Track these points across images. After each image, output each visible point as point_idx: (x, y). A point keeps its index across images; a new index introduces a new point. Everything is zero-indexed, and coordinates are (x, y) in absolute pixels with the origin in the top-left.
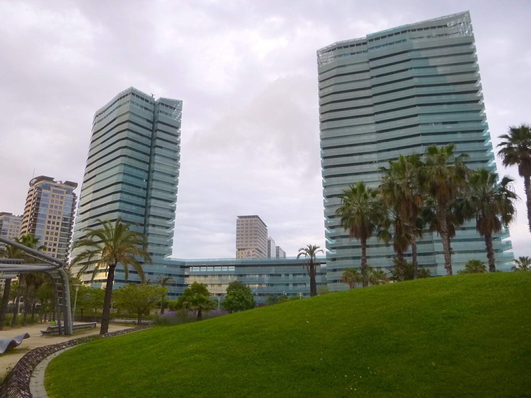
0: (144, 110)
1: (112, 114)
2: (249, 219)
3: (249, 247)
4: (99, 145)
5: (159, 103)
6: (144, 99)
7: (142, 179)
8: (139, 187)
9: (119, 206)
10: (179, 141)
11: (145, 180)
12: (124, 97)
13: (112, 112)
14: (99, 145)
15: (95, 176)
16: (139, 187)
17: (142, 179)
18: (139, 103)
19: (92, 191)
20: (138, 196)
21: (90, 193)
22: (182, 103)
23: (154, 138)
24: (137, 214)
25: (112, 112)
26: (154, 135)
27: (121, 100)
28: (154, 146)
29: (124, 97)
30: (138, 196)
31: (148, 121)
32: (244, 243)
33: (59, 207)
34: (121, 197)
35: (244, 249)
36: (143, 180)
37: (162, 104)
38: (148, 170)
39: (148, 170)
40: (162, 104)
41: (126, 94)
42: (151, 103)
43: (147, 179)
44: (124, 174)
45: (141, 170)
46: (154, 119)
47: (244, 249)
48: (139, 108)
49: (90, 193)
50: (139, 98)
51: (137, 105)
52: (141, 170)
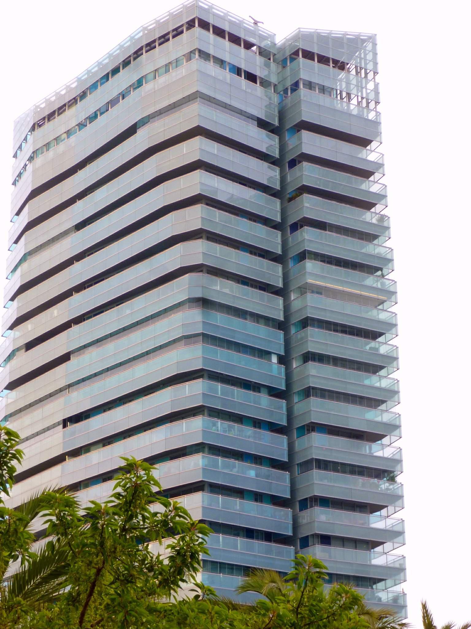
0: (243, 82)
1: (101, 120)
4: (65, 234)
5: (296, 53)
6: (209, 55)
7: (264, 354)
8: (255, 387)
9: (204, 469)
10: (382, 197)
11: (274, 359)
12: (164, 39)
13: (113, 102)
14: (65, 234)
15: (65, 358)
16: (255, 387)
17: (264, 354)
18: (227, 58)
19: (61, 417)
20: (257, 423)
21: (54, 426)
22: (267, 105)
23: (291, 189)
24: (258, 497)
25: (113, 102)
26: (289, 179)
27: (84, 101)
28: (292, 220)
29: (164, 39)
30: (257, 423)
31: (262, 124)
33: (262, 593)
34: (205, 432)
36: (270, 360)
37: (309, 55)
38: (282, 318)
39: (282, 318)
40: (309, 55)
41: (79, 92)
42: (263, 52)
43: (283, 353)
44: (207, 338)
45: (257, 318)
46: (282, 115)
48: (227, 75)
49: (54, 426)
50: (224, 37)
51: (221, 63)
52: (257, 318)
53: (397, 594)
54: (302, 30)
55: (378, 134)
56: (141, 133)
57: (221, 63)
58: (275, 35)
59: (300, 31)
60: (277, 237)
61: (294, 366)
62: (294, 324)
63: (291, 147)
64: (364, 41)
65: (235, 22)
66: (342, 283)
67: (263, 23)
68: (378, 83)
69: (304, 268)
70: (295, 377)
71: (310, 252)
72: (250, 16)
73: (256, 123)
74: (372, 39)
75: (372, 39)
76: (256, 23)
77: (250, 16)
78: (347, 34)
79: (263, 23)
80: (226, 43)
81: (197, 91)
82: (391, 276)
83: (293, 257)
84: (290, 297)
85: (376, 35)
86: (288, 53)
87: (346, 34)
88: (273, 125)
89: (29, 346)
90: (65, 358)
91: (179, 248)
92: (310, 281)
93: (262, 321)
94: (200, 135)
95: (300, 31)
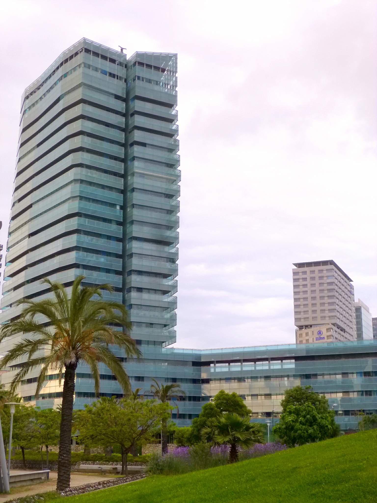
0: (107, 77)
2: (317, 268)
3: (319, 321)
4: (33, 149)
7: (113, 205)
8: (109, 221)
11: (118, 207)
12: (71, 57)
13: (52, 88)
14: (33, 149)
15: (30, 206)
16: (109, 221)
17: (113, 205)
18: (99, 66)
19: (27, 233)
20: (109, 238)
21: (24, 238)
24: (108, 271)
25: (52, 88)
28: (130, 142)
29: (71, 57)
30: (109, 238)
31: (117, 97)
32: (310, 315)
34: (78, 242)
35: (311, 326)
36: (116, 208)
37: (141, 64)
38: (123, 188)
39: (123, 188)
40: (141, 64)
42: (120, 64)
44: (81, 198)
45: (111, 188)
46: (128, 93)
47: (311, 326)
48: (99, 75)
49: (24, 238)
50: (98, 57)
51: (96, 69)
52: (111, 188)
53: (172, 314)
54: (138, 52)
55: (176, 101)
56: (61, 102)
57: (96, 69)
58: (126, 55)
59: (137, 53)
60: (122, 150)
61: (128, 210)
62: (129, 191)
63: (131, 107)
64: (171, 57)
65: (105, 49)
66: (153, 171)
67: (126, 49)
68: (177, 77)
69: (133, 164)
70: (128, 215)
71: (137, 157)
72: (119, 46)
73: (114, 96)
74: (175, 55)
75: (175, 55)
76: (122, 49)
77: (119, 46)
78: (162, 54)
79: (126, 49)
80: (100, 60)
81: (82, 82)
82: (179, 168)
83: (131, 159)
84: (128, 178)
85: (177, 54)
86: (132, 63)
87: (161, 54)
88: (124, 98)
89: (20, 200)
90: (30, 206)
91: (71, 156)
92: (136, 170)
93: (114, 190)
94: (83, 103)
95: (137, 53)
